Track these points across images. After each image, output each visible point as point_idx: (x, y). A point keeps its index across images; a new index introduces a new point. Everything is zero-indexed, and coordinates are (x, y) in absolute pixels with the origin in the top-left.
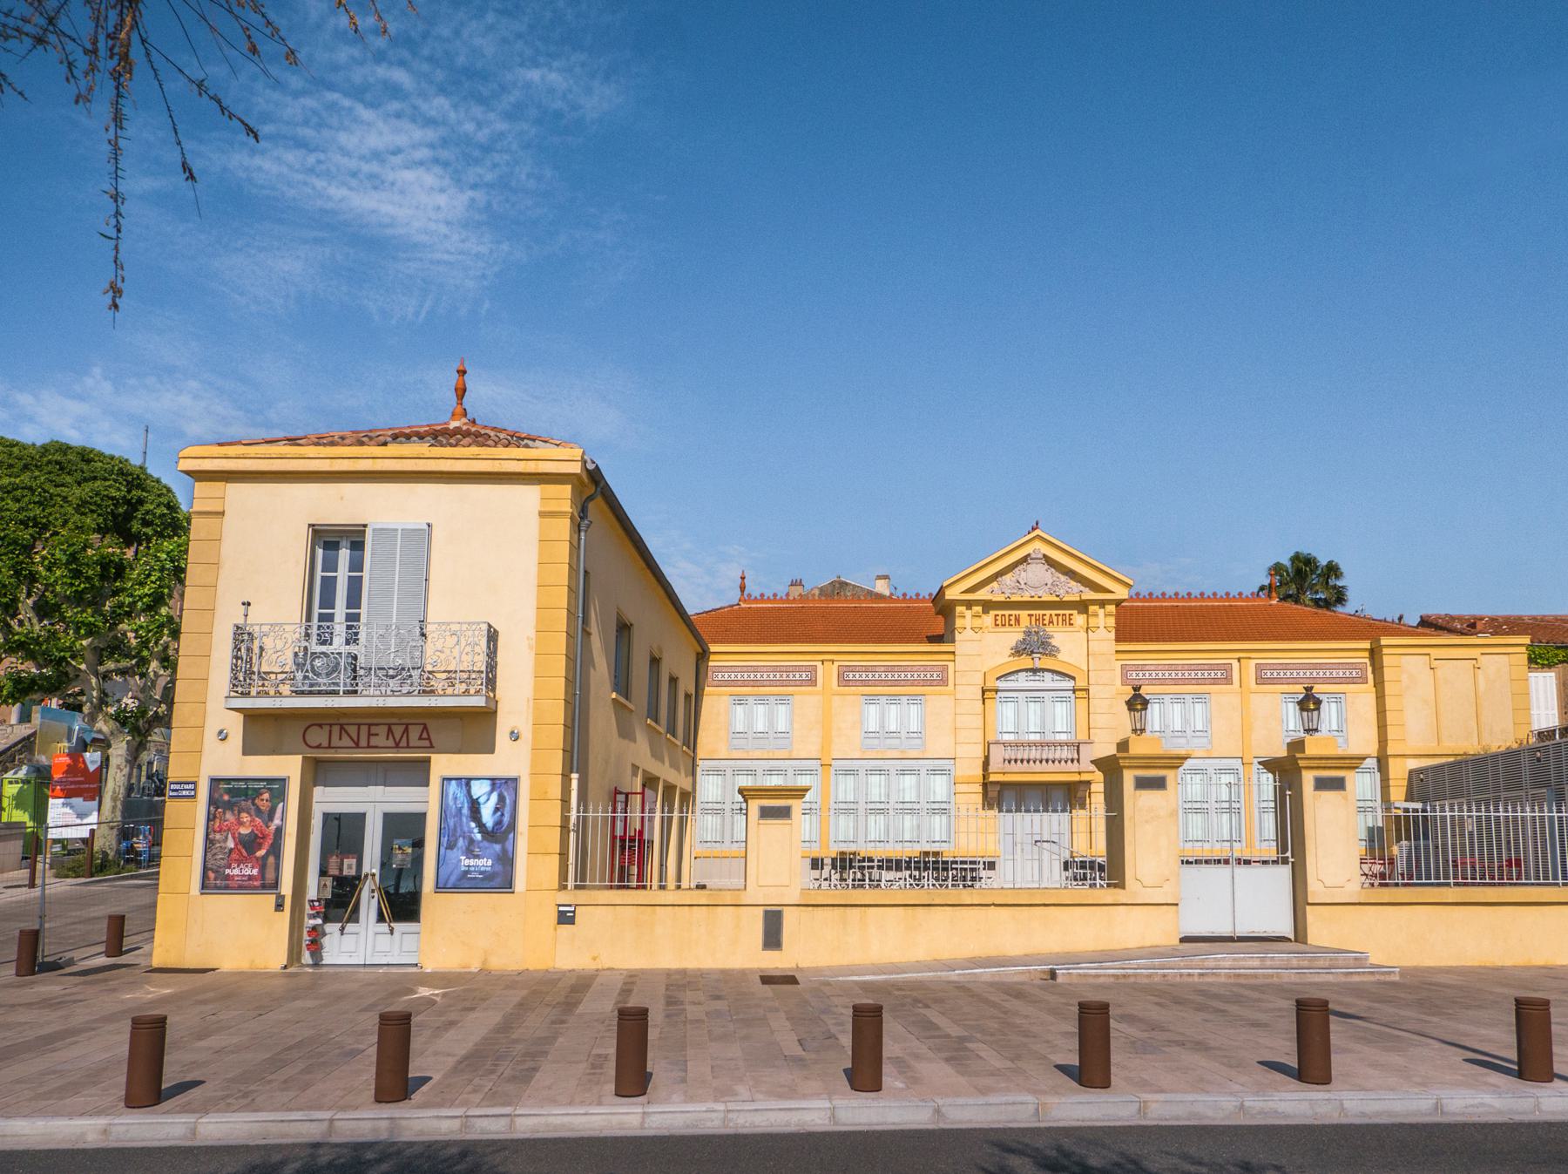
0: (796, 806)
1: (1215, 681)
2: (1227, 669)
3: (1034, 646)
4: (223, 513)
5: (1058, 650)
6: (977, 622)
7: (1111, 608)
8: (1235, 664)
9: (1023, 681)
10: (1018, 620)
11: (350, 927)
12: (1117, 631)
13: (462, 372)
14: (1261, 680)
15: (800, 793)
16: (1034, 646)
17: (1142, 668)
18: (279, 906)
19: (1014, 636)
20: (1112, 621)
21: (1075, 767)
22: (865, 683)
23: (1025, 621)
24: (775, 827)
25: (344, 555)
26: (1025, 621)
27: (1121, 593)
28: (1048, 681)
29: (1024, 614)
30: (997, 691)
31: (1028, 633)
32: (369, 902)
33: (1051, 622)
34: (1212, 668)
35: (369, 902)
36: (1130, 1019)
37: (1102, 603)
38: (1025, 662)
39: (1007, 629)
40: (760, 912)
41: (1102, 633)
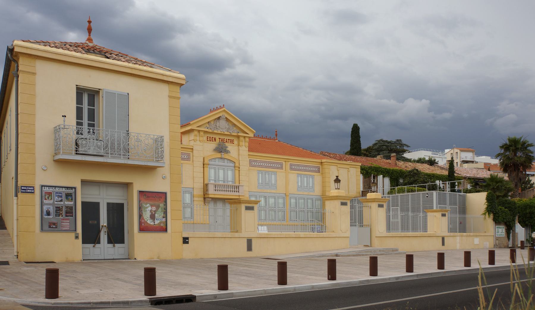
0: (256, 207)
1: (278, 168)
2: (281, 164)
3: (221, 149)
4: (34, 74)
5: (230, 152)
6: (201, 139)
7: (247, 139)
8: (284, 163)
9: (217, 162)
10: (215, 139)
11: (97, 245)
12: (249, 147)
13: (90, 22)
14: (291, 169)
15: (256, 202)
16: (221, 149)
17: (256, 161)
18: (77, 237)
19: (213, 145)
20: (247, 144)
21: (237, 194)
22: (259, 166)
23: (218, 140)
24: (250, 212)
25: (260, 182)
26: (218, 140)
27: (251, 135)
28: (226, 163)
29: (217, 137)
30: (209, 165)
31: (219, 145)
32: (104, 237)
33: (227, 142)
34: (277, 163)
35: (104, 237)
36: (139, 285)
37: (245, 137)
38: (219, 155)
39: (211, 142)
40: (430, 231)
41: (244, 147)
